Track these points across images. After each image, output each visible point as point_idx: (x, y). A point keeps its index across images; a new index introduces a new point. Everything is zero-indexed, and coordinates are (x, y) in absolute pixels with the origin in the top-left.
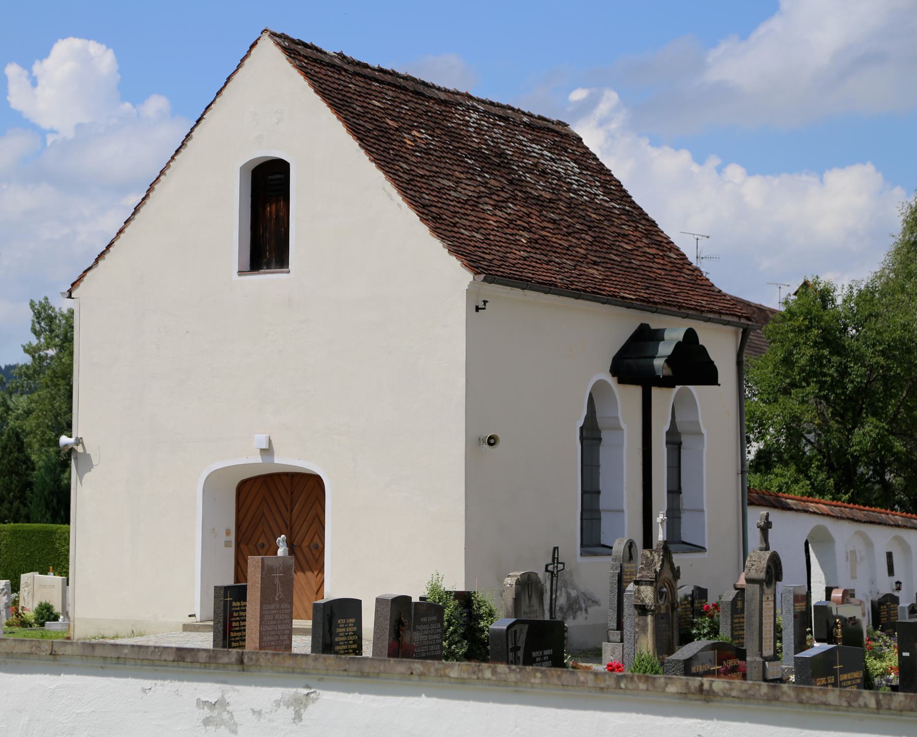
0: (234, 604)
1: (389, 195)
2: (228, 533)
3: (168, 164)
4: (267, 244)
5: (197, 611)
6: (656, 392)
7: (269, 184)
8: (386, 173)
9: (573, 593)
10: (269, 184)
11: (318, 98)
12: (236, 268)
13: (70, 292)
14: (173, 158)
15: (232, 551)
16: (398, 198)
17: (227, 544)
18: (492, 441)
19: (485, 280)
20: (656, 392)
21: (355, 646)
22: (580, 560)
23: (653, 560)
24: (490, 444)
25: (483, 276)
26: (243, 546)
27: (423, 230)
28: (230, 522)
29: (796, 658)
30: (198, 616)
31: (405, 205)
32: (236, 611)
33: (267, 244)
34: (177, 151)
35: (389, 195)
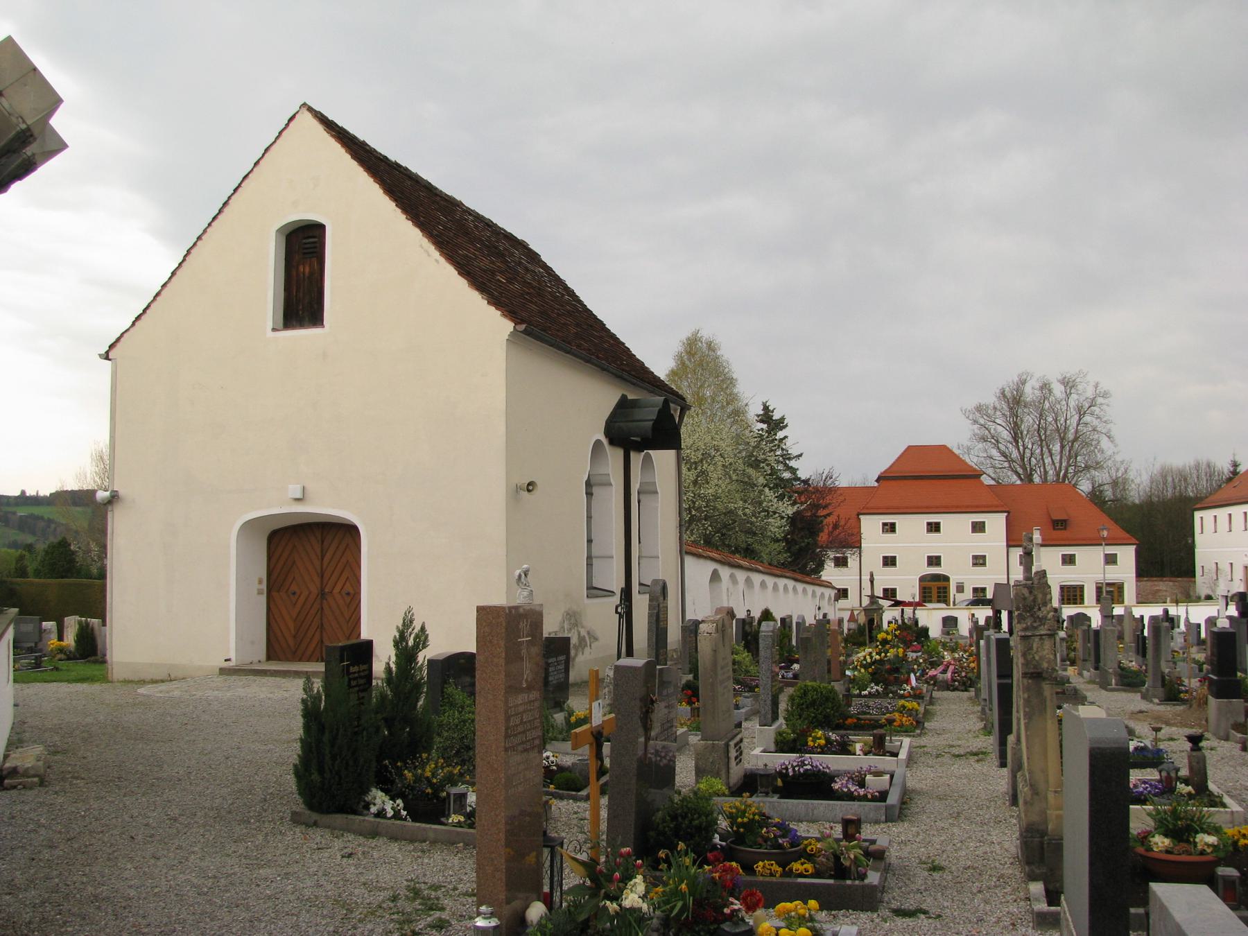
0: (352, 669)
1: (427, 251)
2: (260, 582)
3: (205, 231)
4: (302, 301)
5: (232, 655)
6: (633, 455)
7: (304, 246)
8: (422, 230)
9: (583, 633)
10: (304, 246)
11: (354, 164)
12: (270, 325)
13: (107, 353)
14: (210, 225)
15: (264, 598)
16: (436, 254)
17: (260, 592)
18: (531, 486)
19: (525, 332)
20: (633, 455)
21: (362, 681)
22: (587, 601)
23: (1034, 601)
24: (529, 491)
25: (523, 327)
26: (274, 594)
27: (462, 283)
28: (263, 572)
29: (616, 667)
30: (234, 659)
31: (442, 260)
32: (355, 679)
33: (302, 301)
34: (214, 218)
35: (427, 251)
